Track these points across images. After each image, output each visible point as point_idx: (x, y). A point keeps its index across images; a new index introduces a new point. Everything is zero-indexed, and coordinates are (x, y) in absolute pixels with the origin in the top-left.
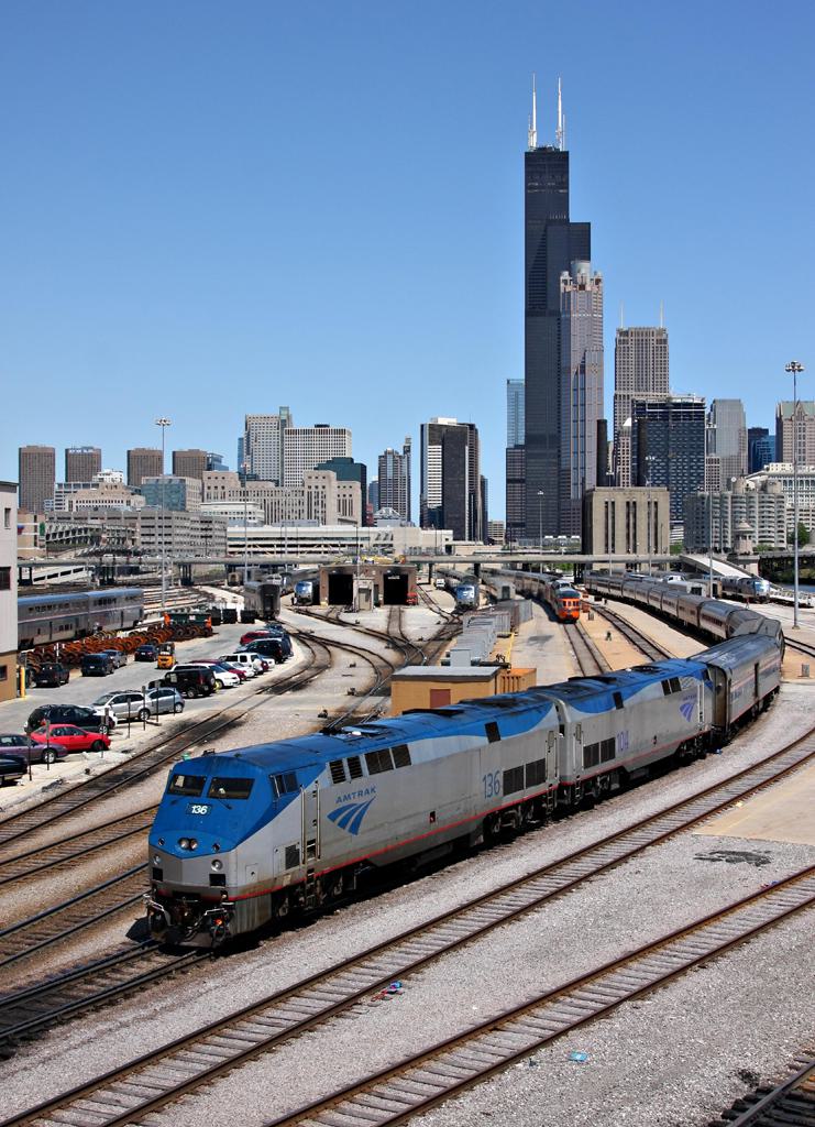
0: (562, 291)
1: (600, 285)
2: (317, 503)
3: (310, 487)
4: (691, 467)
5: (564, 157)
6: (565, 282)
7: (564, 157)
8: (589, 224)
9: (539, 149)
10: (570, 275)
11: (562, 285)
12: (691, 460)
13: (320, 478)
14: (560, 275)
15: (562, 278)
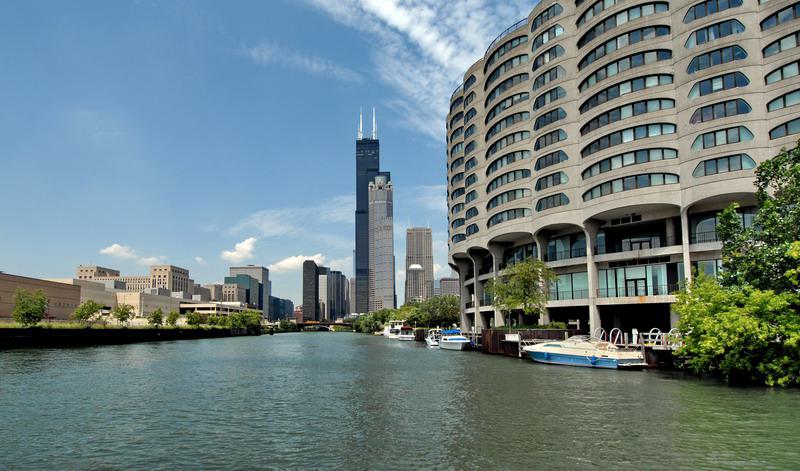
5: (376, 143)
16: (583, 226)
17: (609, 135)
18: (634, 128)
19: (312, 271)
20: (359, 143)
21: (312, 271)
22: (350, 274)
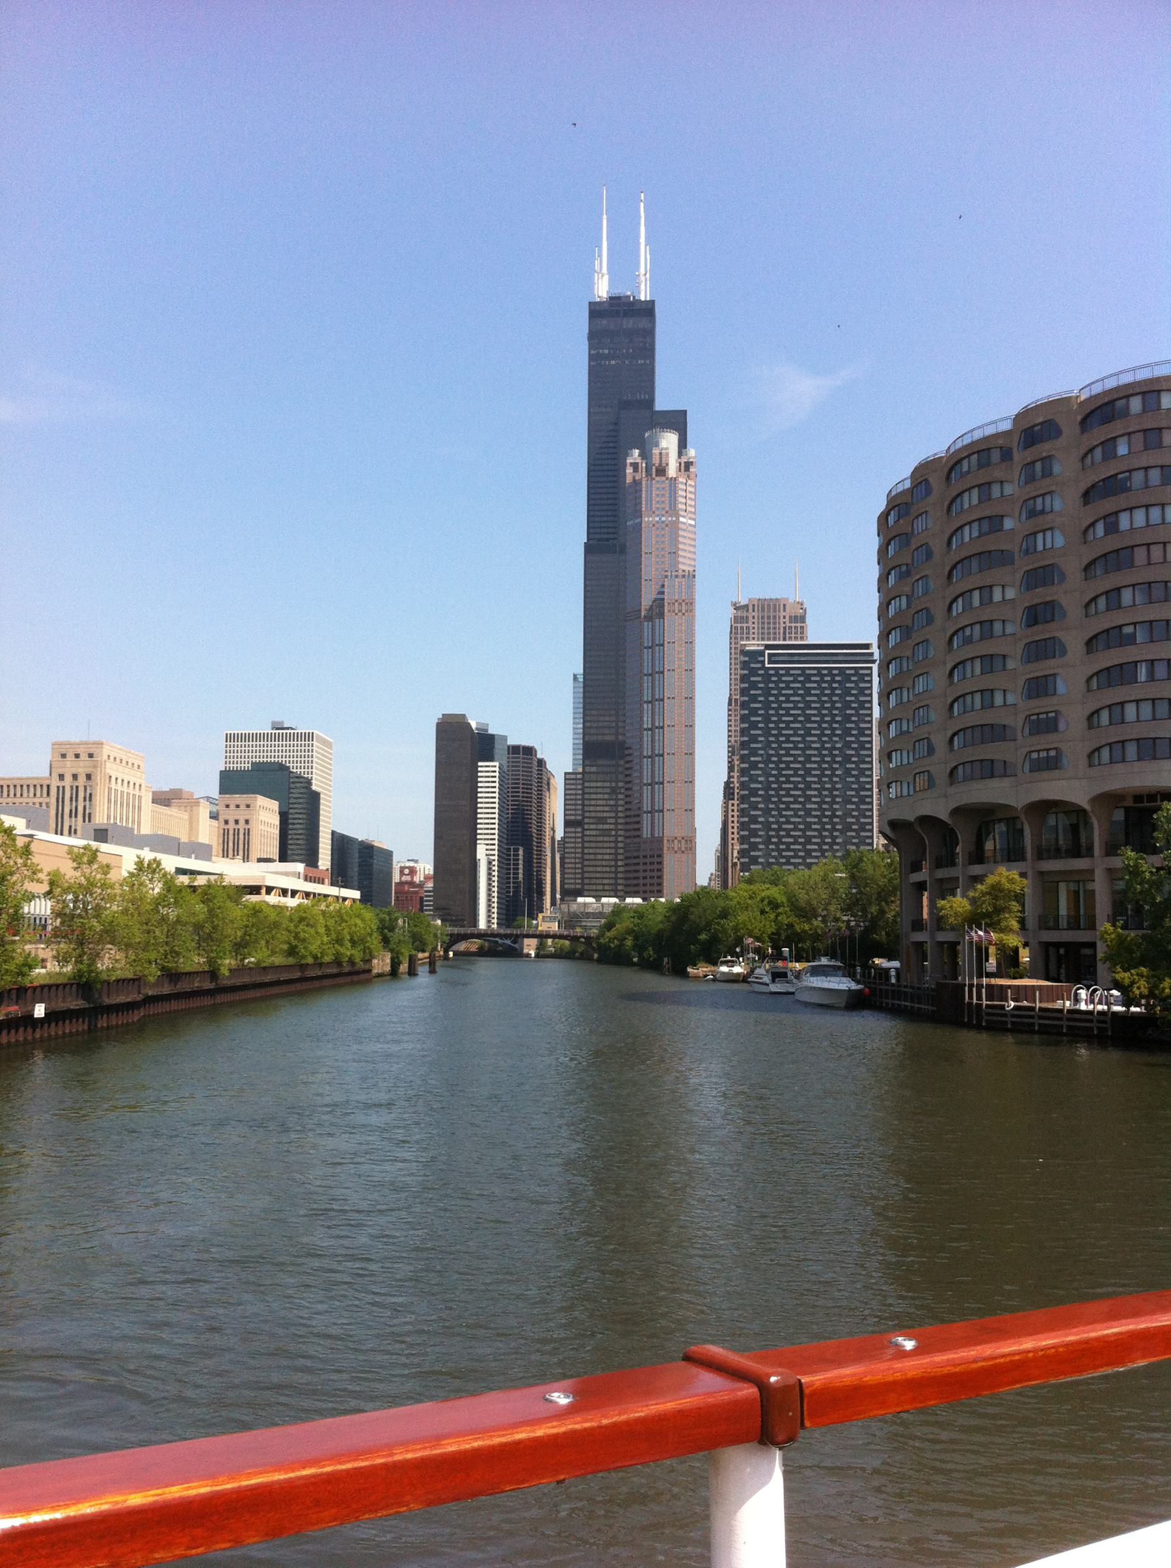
0: (629, 479)
1: (692, 469)
2: (74, 813)
3: (61, 777)
4: (848, 745)
5: (647, 310)
6: (635, 466)
7: (647, 310)
8: (685, 412)
9: (611, 298)
10: (643, 455)
11: (629, 470)
12: (847, 718)
13: (232, 807)
14: (627, 455)
15: (629, 461)
16: (1087, 807)
17: (1121, 665)
18: (1109, 706)
19: (461, 747)
20: (597, 311)
21: (461, 747)
22: (560, 756)
